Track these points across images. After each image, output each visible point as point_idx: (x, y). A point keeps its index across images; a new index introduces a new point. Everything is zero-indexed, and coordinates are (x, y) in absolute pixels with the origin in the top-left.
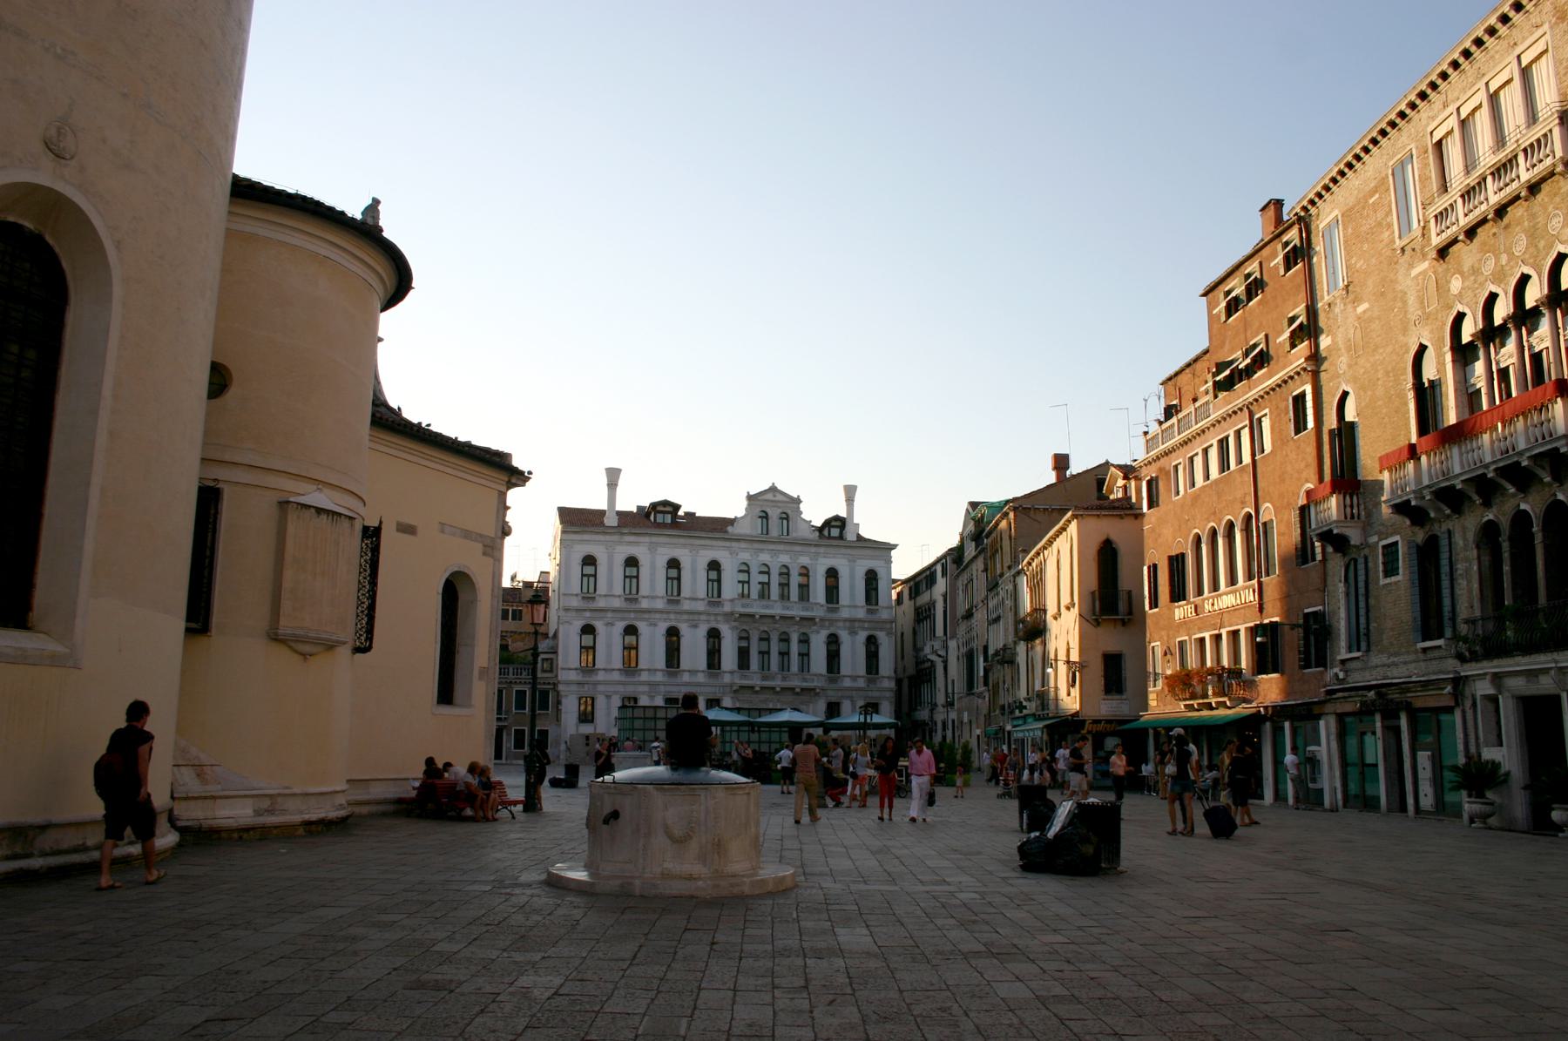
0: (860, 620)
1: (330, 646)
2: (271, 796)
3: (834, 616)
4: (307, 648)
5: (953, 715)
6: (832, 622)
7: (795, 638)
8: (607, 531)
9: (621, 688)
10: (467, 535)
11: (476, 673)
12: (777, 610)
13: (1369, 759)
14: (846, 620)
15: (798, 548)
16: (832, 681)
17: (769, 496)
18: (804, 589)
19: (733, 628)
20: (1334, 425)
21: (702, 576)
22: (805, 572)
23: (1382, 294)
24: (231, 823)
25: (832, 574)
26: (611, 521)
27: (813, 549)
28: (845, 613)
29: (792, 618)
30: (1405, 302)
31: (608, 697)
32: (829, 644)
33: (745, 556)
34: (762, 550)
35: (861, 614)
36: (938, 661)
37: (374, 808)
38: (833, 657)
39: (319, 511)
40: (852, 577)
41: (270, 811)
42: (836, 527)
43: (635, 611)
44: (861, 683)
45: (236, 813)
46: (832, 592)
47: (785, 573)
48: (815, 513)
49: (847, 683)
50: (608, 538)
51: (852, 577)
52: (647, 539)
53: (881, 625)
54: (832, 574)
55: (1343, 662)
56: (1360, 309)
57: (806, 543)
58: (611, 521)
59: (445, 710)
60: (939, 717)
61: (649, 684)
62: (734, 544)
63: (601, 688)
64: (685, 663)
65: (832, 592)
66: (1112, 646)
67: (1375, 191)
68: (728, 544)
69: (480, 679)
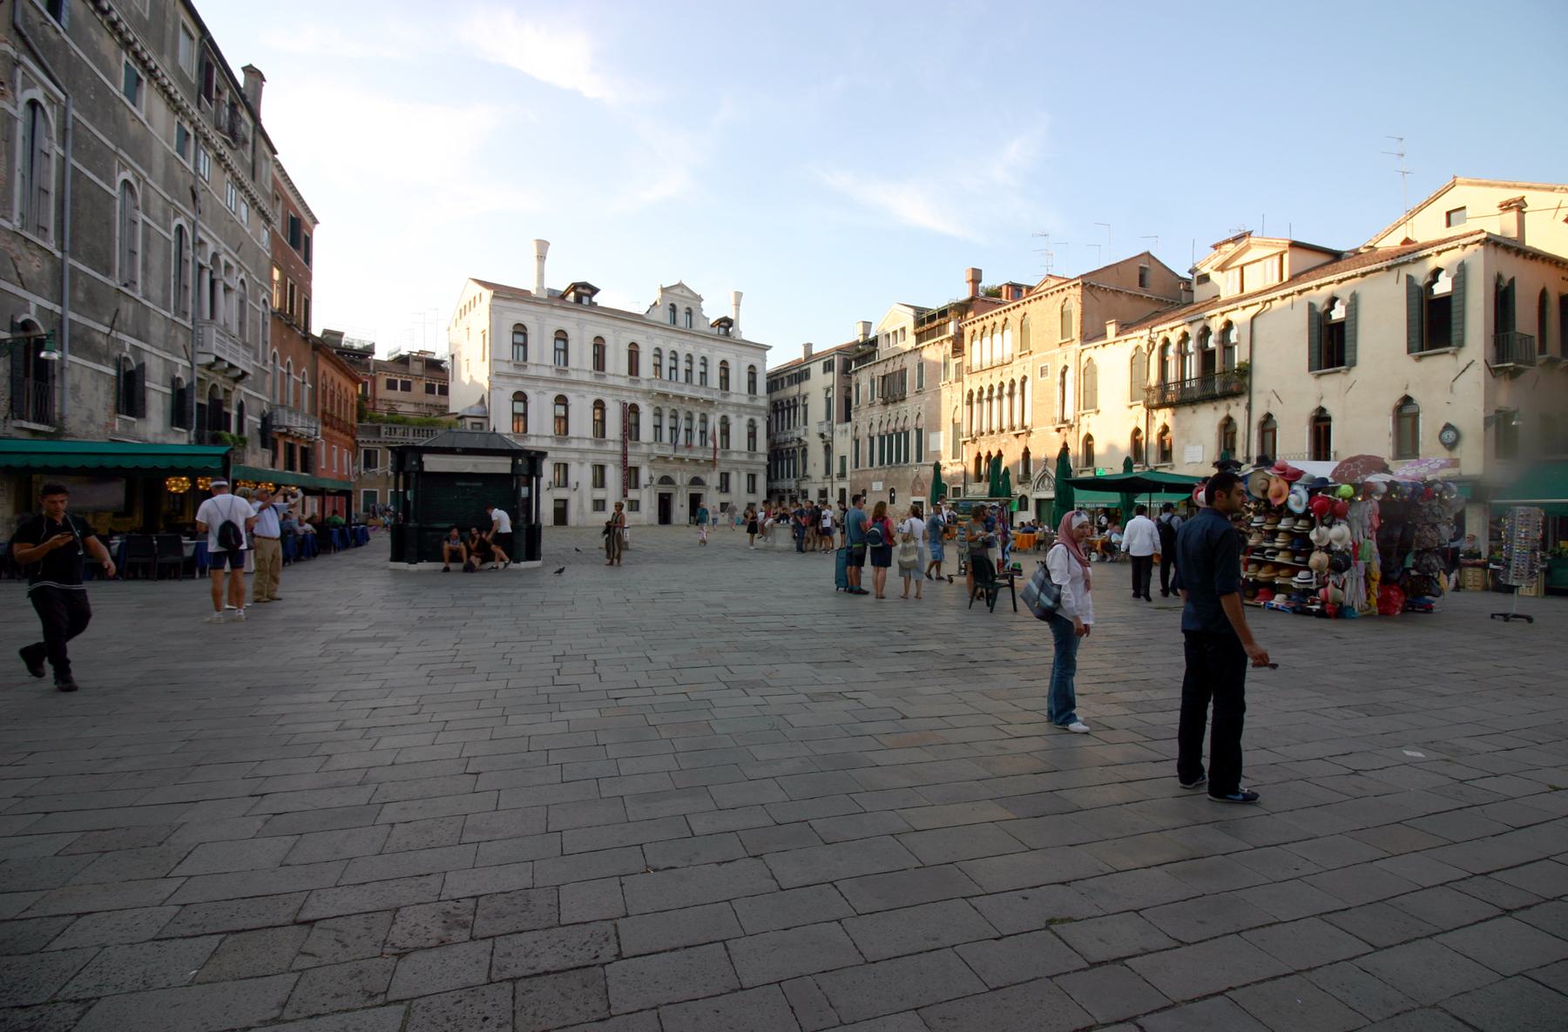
28: (733, 399)
33: (659, 343)
35: (745, 400)
42: (725, 323)
62: (650, 330)
68: (644, 328)
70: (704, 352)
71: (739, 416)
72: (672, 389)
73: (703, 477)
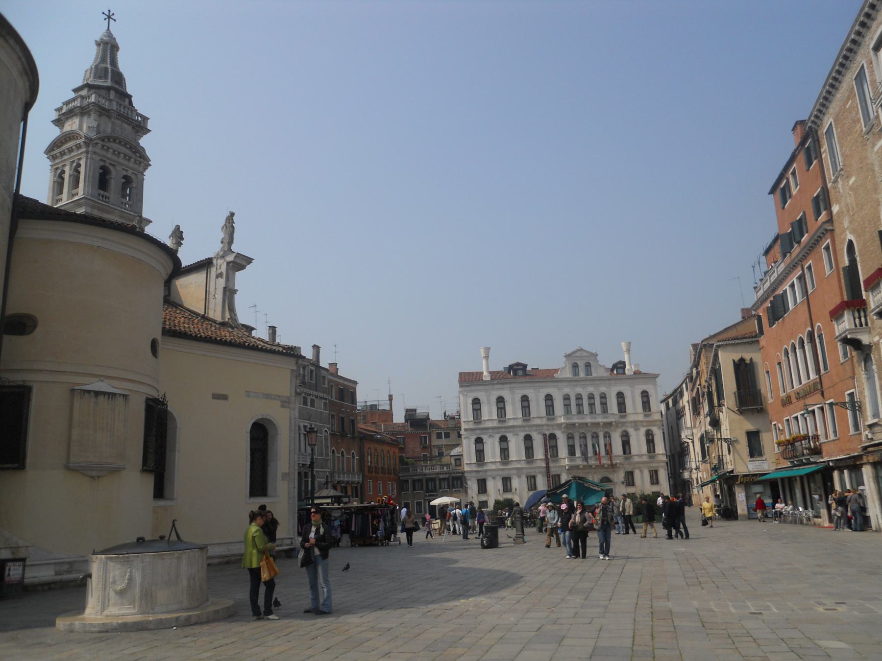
0: (640, 422)
1: (115, 471)
2: (69, 563)
3: (624, 420)
4: (94, 474)
5: (700, 475)
6: (623, 424)
7: (601, 435)
8: (485, 383)
9: (501, 472)
10: (268, 396)
11: (279, 476)
12: (588, 420)
13: (405, 534)
14: (631, 422)
15: (598, 382)
16: (626, 459)
17: (578, 354)
18: (604, 404)
19: (563, 432)
20: (847, 263)
21: (519, 405)
22: (603, 397)
23: (861, 168)
24: (36, 580)
25: (620, 395)
26: (486, 377)
27: (607, 382)
28: (631, 418)
29: (599, 423)
30: (873, 171)
31: (641, 471)
32: (622, 436)
34: (576, 386)
35: (641, 417)
36: (691, 444)
37: (221, 560)
38: (626, 444)
39: (97, 394)
40: (633, 396)
41: (68, 572)
43: (529, 426)
44: (645, 459)
45: (45, 574)
46: (622, 406)
47: (591, 397)
48: (607, 360)
49: (636, 459)
50: (486, 387)
51: (633, 396)
52: (508, 386)
53: (653, 423)
54: (620, 395)
55: (871, 426)
56: (851, 182)
57: (601, 379)
58: (486, 377)
59: (161, 503)
60: (694, 476)
61: (517, 469)
63: (489, 473)
64: (634, 450)
65: (622, 406)
66: (751, 427)
67: (848, 99)
68: (555, 384)
69: (283, 479)
70: (603, 389)
71: (637, 429)
72: (576, 420)
73: (610, 476)
